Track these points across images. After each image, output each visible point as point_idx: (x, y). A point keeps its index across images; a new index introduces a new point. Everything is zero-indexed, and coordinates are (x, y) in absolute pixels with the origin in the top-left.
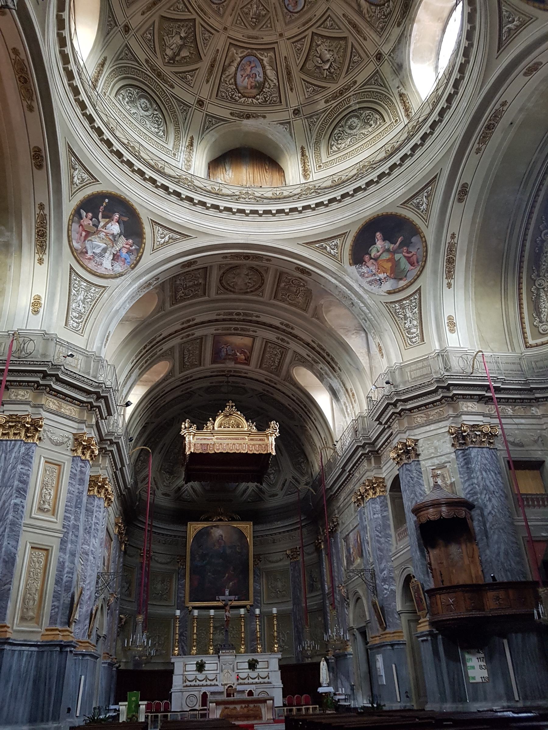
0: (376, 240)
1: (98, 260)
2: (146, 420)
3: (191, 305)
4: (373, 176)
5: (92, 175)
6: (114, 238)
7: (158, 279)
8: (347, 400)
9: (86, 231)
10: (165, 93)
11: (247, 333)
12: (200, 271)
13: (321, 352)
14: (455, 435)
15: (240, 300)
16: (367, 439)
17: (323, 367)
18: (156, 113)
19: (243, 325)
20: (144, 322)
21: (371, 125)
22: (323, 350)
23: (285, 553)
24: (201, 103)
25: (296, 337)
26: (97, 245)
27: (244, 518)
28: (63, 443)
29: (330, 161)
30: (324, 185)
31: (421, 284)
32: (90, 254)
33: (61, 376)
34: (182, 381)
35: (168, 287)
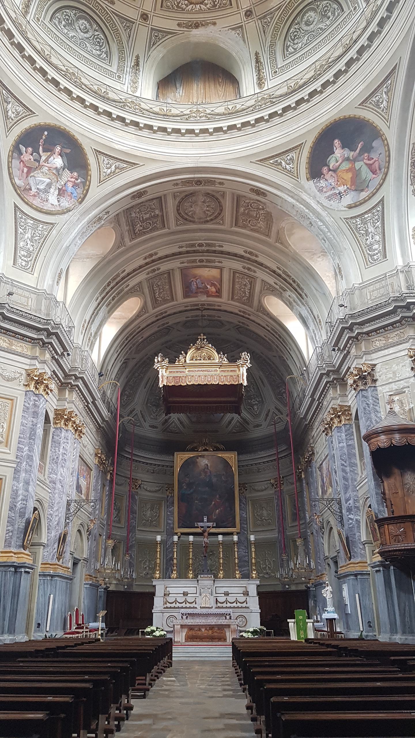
0: (335, 148)
1: (43, 196)
2: (125, 355)
3: (152, 239)
4: (329, 76)
5: (27, 108)
6: (58, 172)
7: (108, 212)
8: (315, 327)
9: (27, 167)
10: (105, 10)
11: (213, 264)
12: (155, 201)
13: (288, 279)
14: (413, 358)
15: (201, 230)
16: (331, 367)
17: (289, 294)
18: (97, 33)
19: (208, 256)
20: (104, 258)
21: (329, 18)
22: (288, 276)
23: (269, 482)
24: (145, 17)
25: (262, 265)
26: (41, 181)
27: (228, 448)
28: (15, 379)
29: (286, 65)
30: (279, 93)
31: (384, 194)
32: (34, 190)
33: (6, 314)
34: (157, 316)
35: (123, 220)
